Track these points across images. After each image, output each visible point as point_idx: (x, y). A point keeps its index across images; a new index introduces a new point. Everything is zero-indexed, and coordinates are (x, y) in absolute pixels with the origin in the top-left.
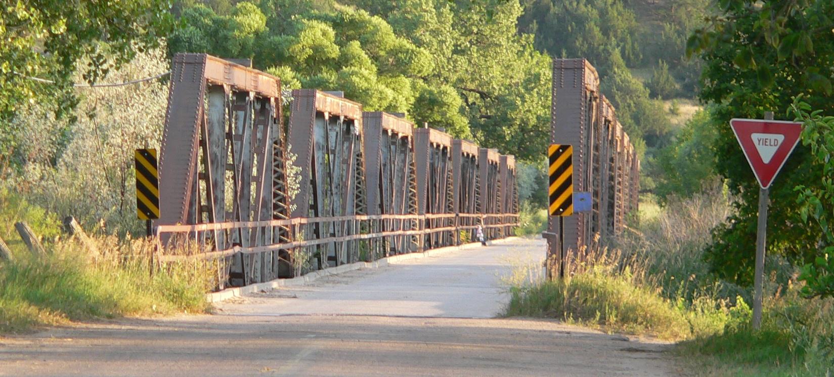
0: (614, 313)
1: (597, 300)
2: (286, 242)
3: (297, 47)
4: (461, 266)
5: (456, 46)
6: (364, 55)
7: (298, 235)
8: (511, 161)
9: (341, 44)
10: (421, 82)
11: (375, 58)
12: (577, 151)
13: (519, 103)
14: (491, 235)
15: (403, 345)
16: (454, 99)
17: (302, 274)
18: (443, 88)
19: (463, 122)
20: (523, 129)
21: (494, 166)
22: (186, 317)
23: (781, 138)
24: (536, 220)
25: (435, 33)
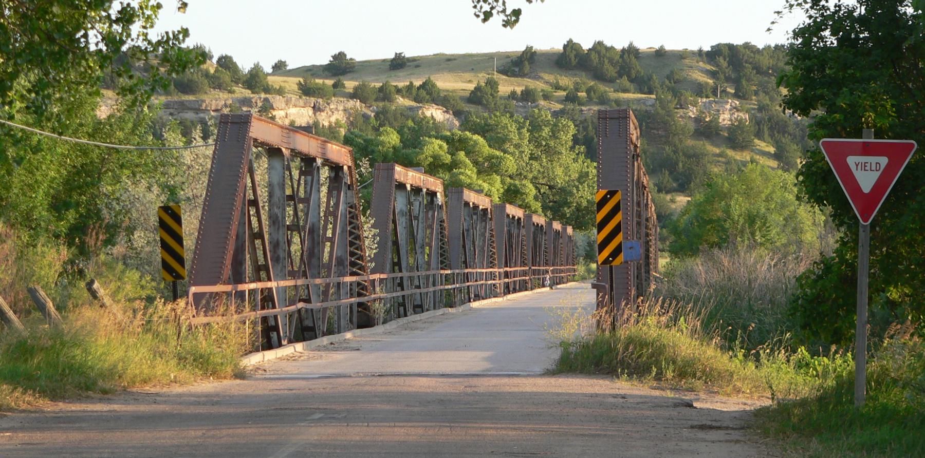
0: (671, 367)
1: (652, 355)
2: (365, 295)
3: (422, 157)
4: (526, 308)
5: (531, 154)
6: (467, 161)
7: (378, 289)
8: (570, 230)
9: (452, 155)
10: (508, 179)
11: (476, 163)
12: (625, 194)
13: (575, 191)
14: (555, 283)
15: (421, 431)
16: (531, 190)
17: (383, 323)
18: (524, 182)
19: (537, 206)
20: (578, 209)
21: (557, 232)
22: (208, 386)
23: (884, 161)
24: (589, 271)
25: (517, 146)
